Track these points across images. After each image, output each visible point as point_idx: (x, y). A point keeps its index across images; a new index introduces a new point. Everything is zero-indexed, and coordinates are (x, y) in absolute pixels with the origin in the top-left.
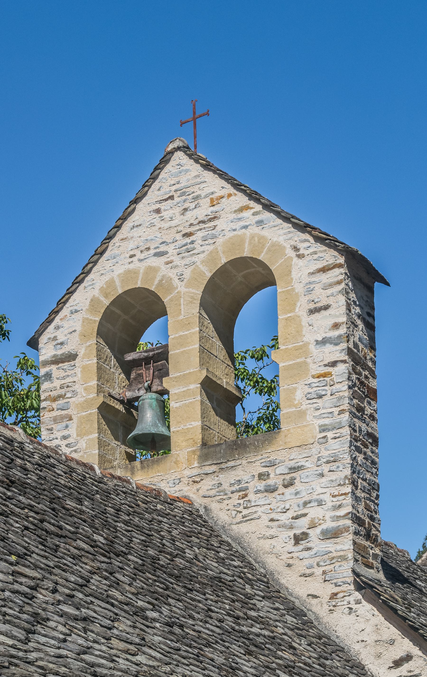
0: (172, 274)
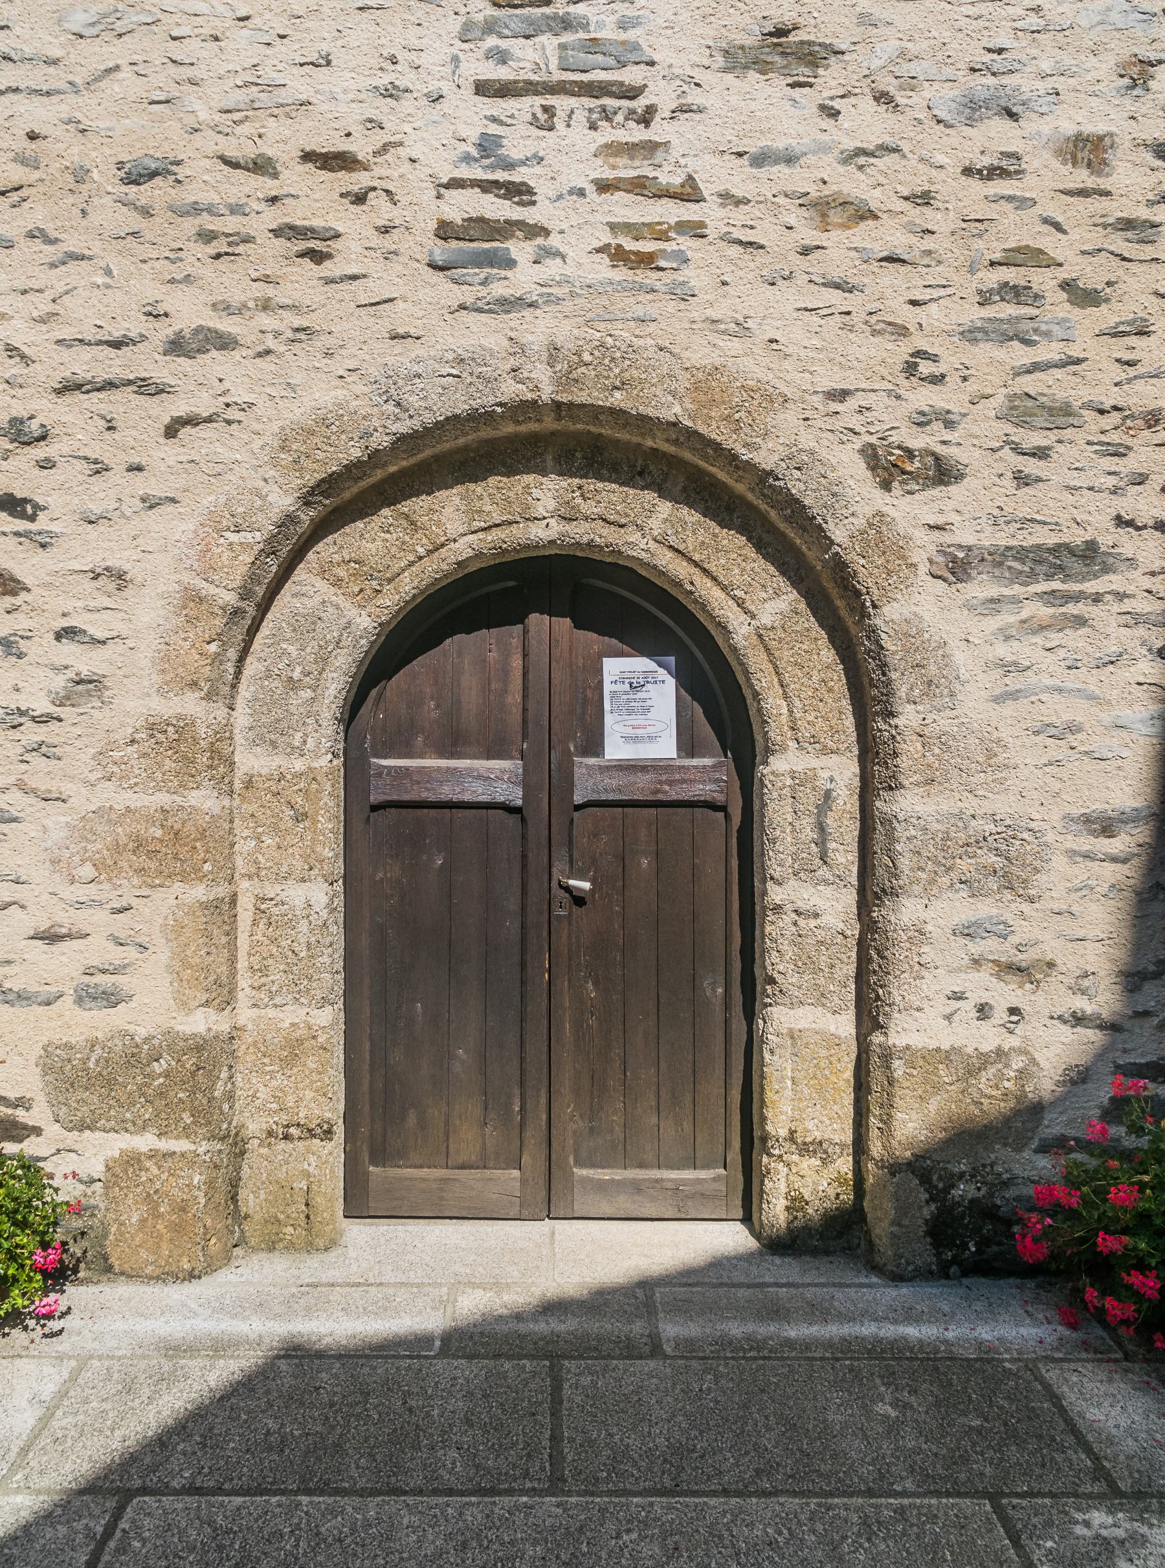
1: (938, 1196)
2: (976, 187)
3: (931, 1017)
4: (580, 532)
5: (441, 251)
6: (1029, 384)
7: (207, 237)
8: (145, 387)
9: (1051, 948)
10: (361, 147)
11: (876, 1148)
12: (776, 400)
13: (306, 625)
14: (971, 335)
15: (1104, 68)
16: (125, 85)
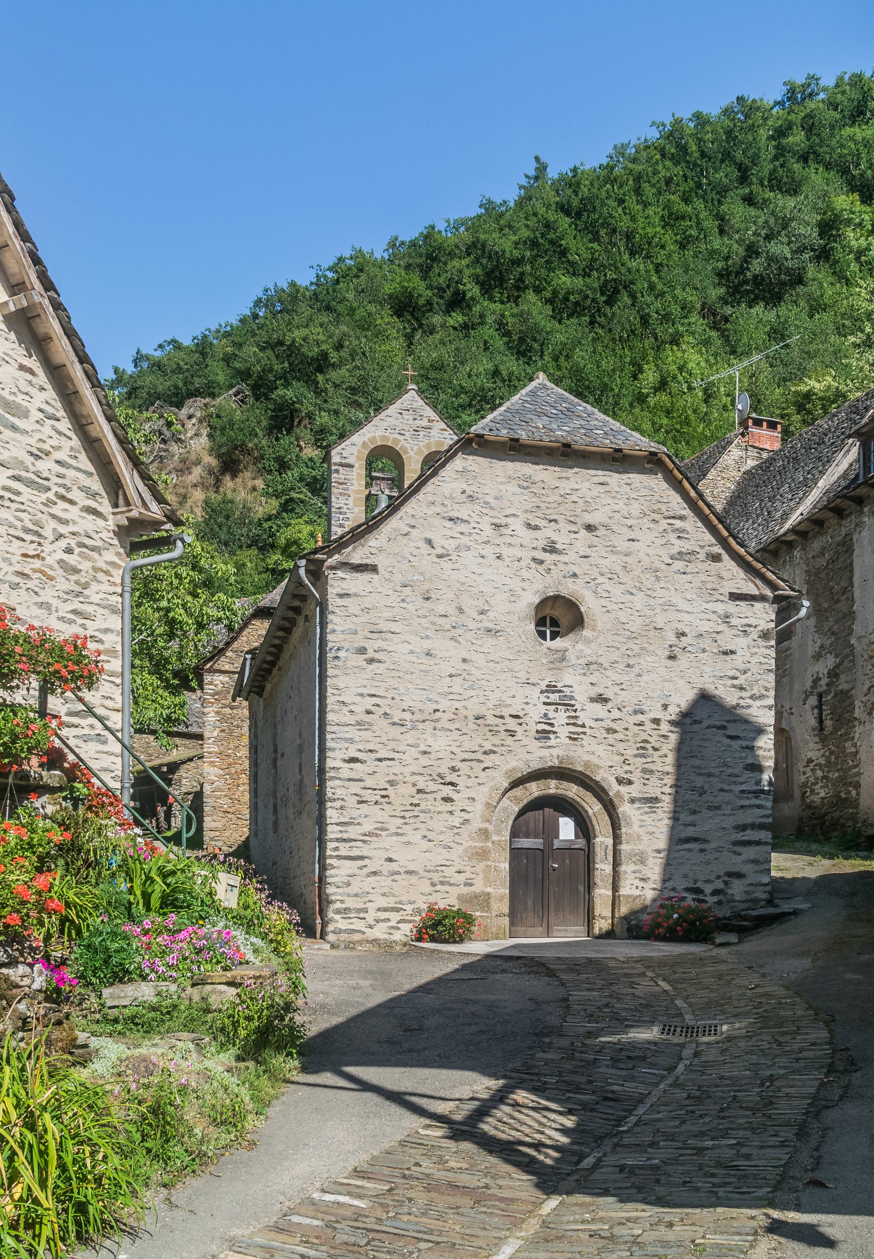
0: (407, 446)
1: (629, 923)
2: (636, 727)
3: (627, 889)
4: (560, 792)
5: (537, 736)
6: (646, 766)
7: (491, 731)
8: (479, 761)
9: (649, 875)
10: (521, 714)
11: (617, 915)
12: (599, 767)
13: (505, 809)
14: (635, 756)
15: (659, 705)
16: (475, 699)
